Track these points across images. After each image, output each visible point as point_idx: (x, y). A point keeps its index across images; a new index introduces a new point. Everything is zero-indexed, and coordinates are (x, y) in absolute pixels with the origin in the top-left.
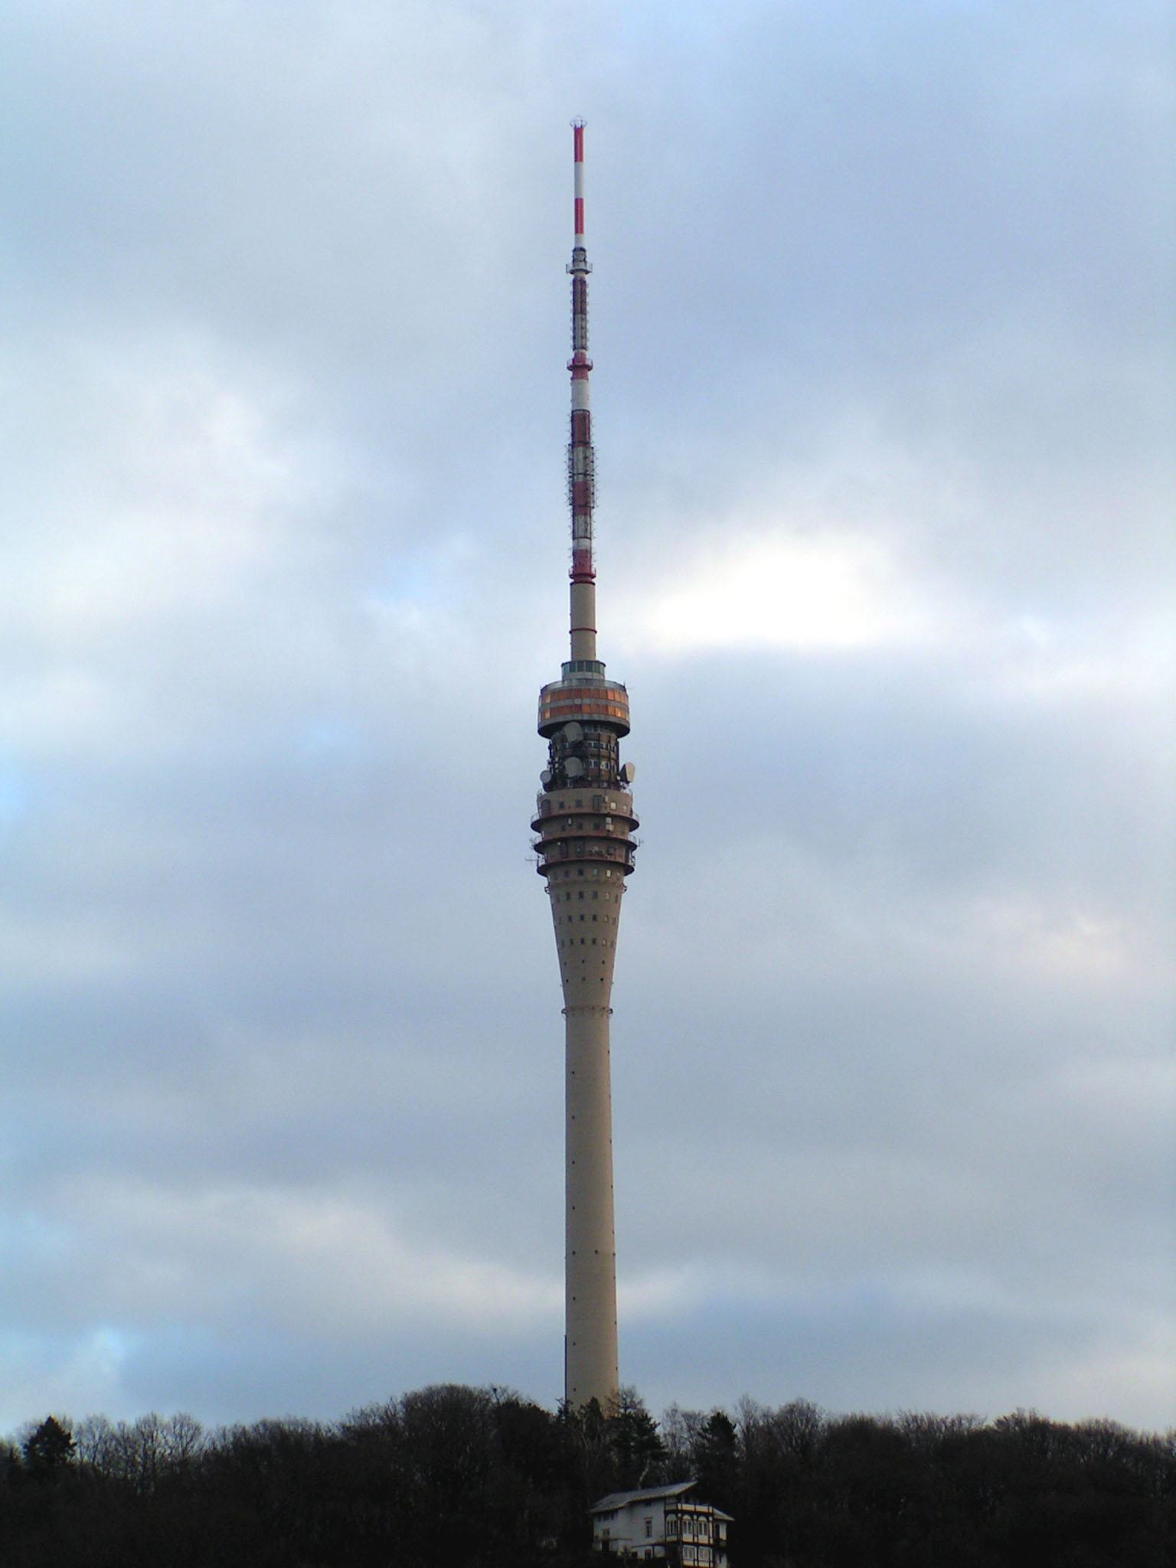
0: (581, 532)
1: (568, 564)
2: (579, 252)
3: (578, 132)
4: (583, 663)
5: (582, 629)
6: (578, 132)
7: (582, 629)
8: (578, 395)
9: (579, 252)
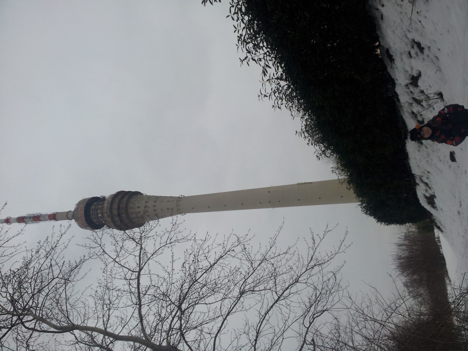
7: (67, 216)
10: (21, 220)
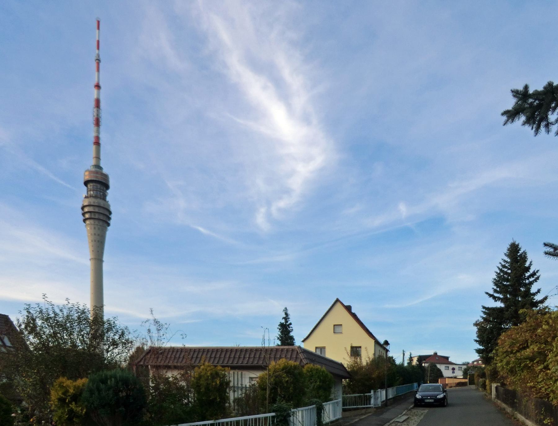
0: (98, 132)
2: (98, 55)
3: (99, 22)
4: (98, 166)
5: (98, 158)
6: (99, 22)
7: (98, 158)
8: (98, 94)
9: (98, 55)
10: (98, 102)
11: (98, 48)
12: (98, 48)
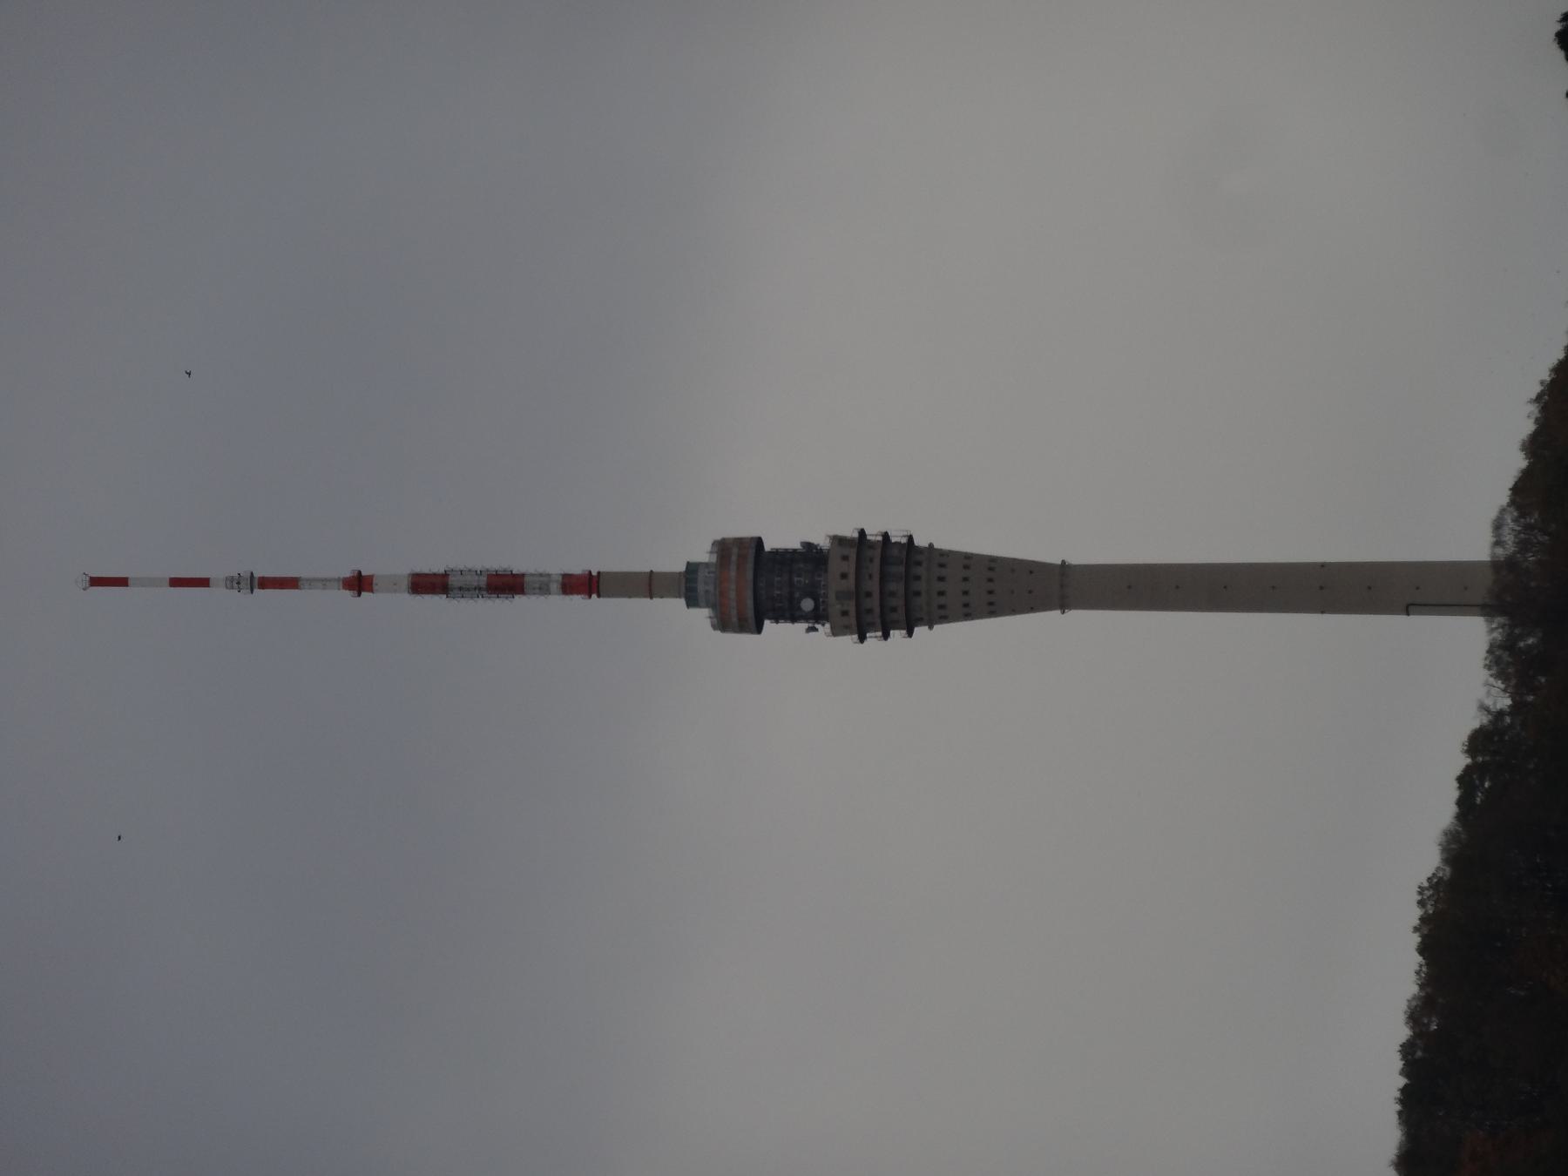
1: (577, 600)
2: (235, 583)
3: (96, 582)
6: (96, 582)
7: (650, 585)
9: (235, 583)
11: (204, 582)
12: (204, 582)
